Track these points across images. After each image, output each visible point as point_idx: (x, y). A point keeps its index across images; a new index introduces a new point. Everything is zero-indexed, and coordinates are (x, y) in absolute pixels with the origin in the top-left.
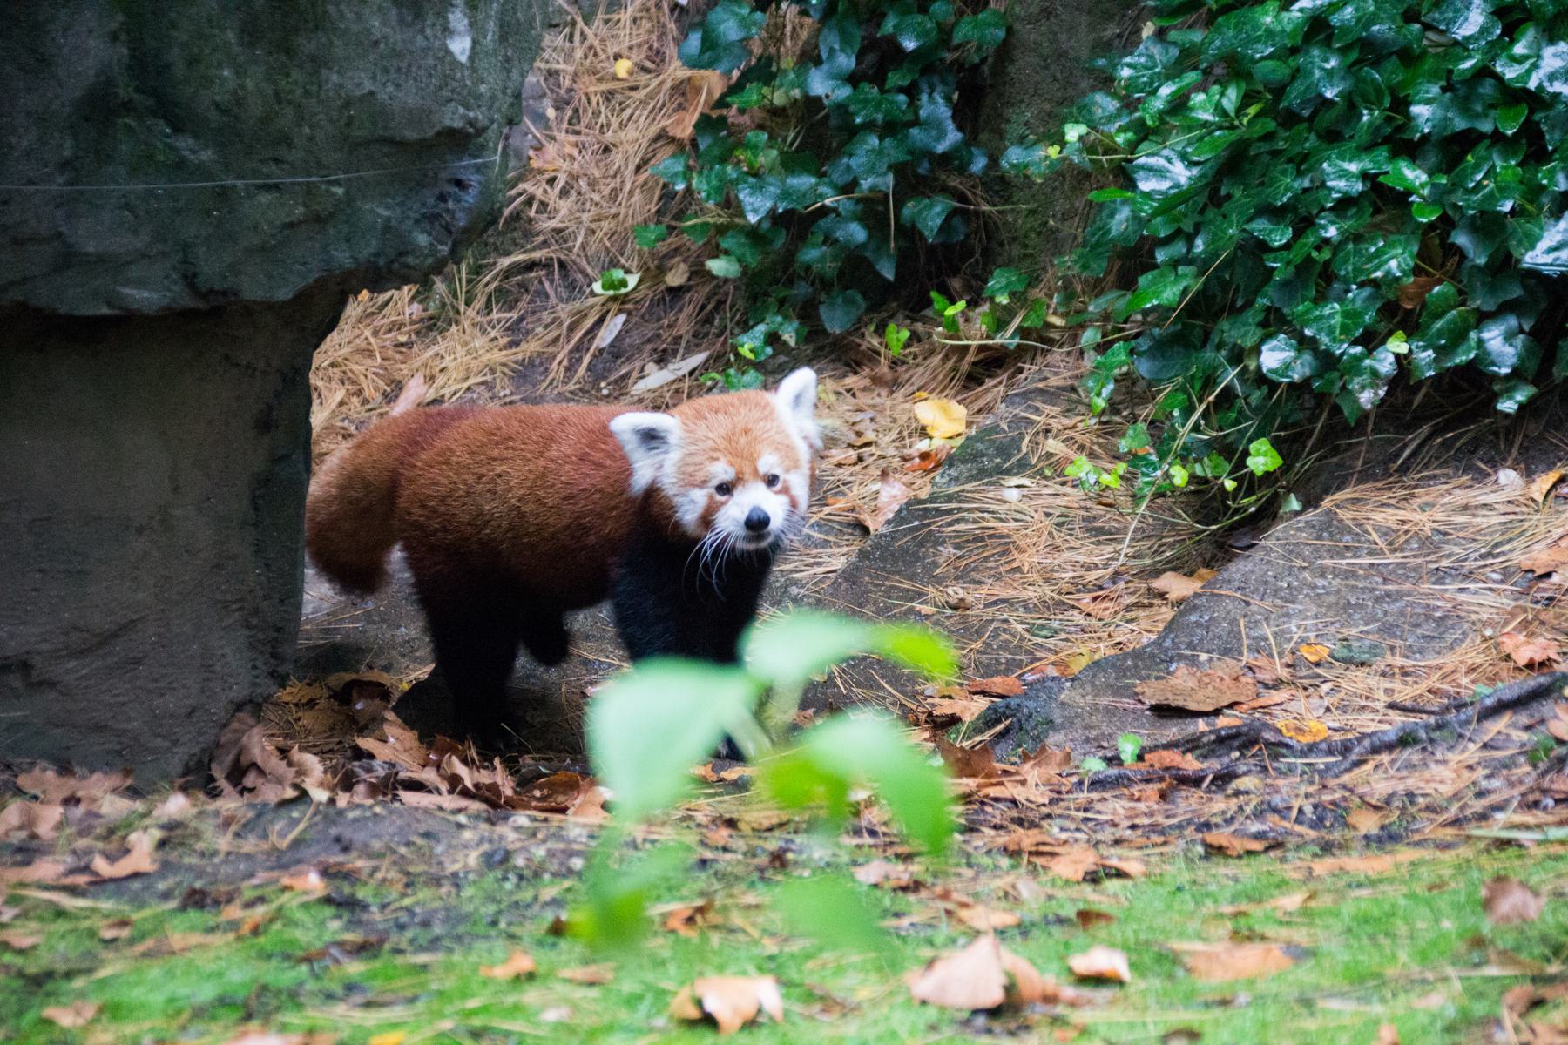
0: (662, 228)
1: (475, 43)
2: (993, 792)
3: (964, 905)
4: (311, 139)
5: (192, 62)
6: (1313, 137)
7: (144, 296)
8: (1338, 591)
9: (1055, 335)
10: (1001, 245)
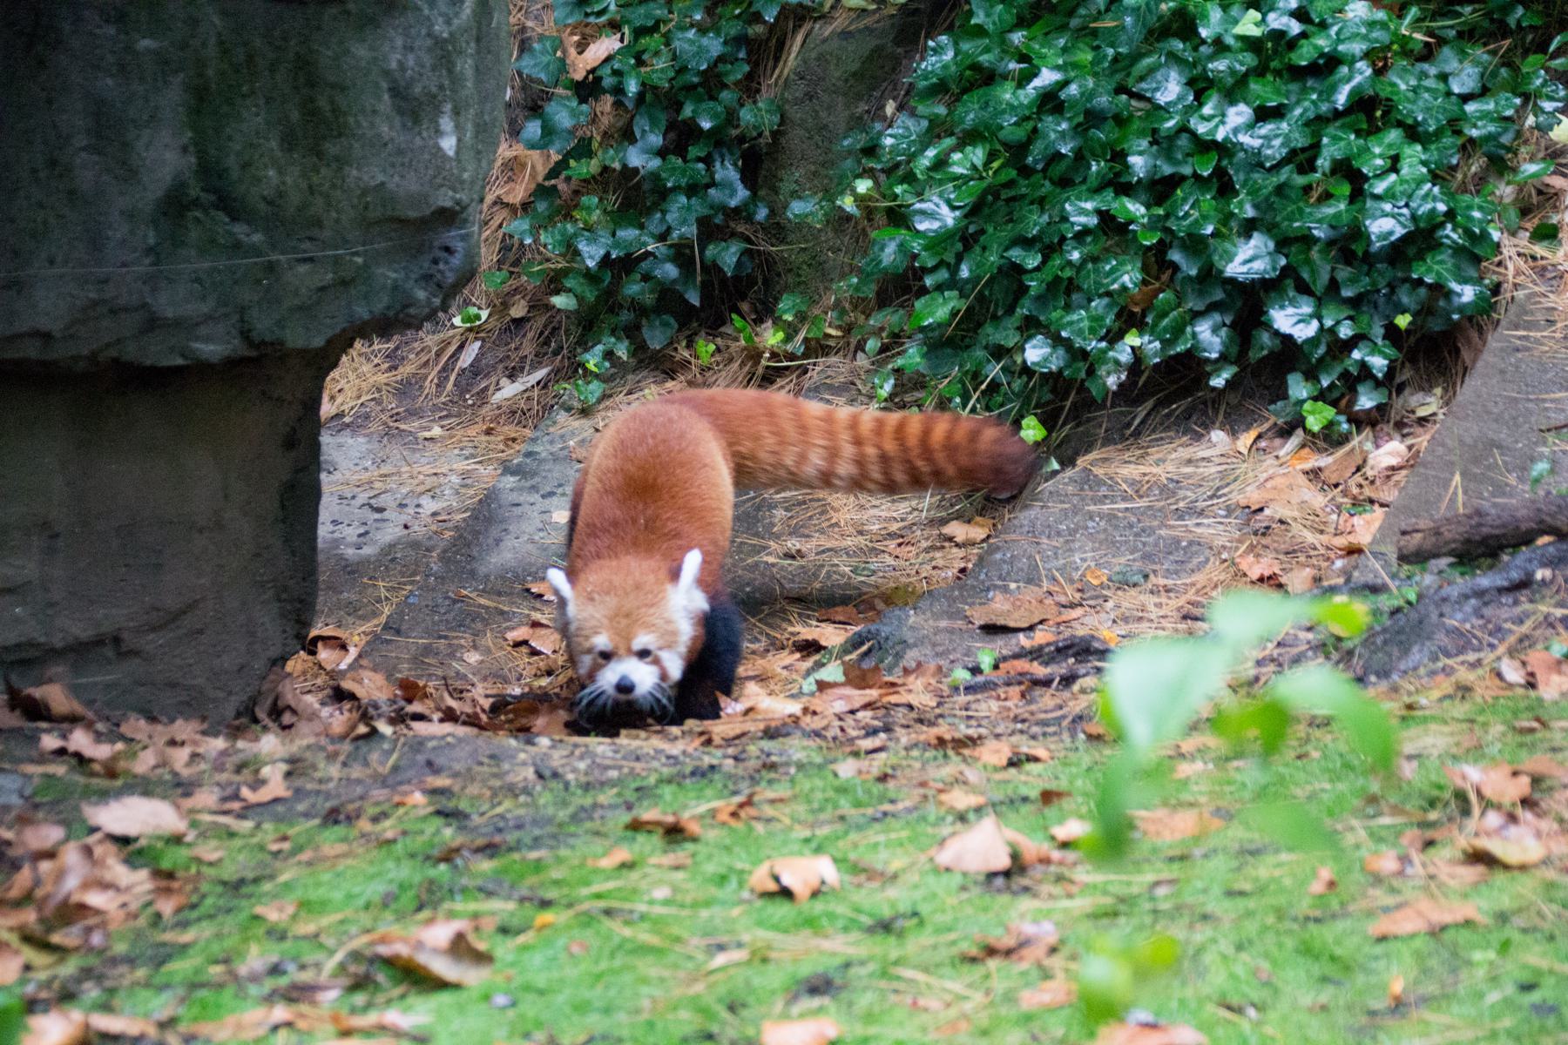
0: (505, 273)
1: (459, 140)
2: (893, 699)
3: (941, 791)
4: (337, 221)
5: (245, 166)
6: (1047, 183)
7: (212, 349)
9: (832, 343)
10: (779, 275)
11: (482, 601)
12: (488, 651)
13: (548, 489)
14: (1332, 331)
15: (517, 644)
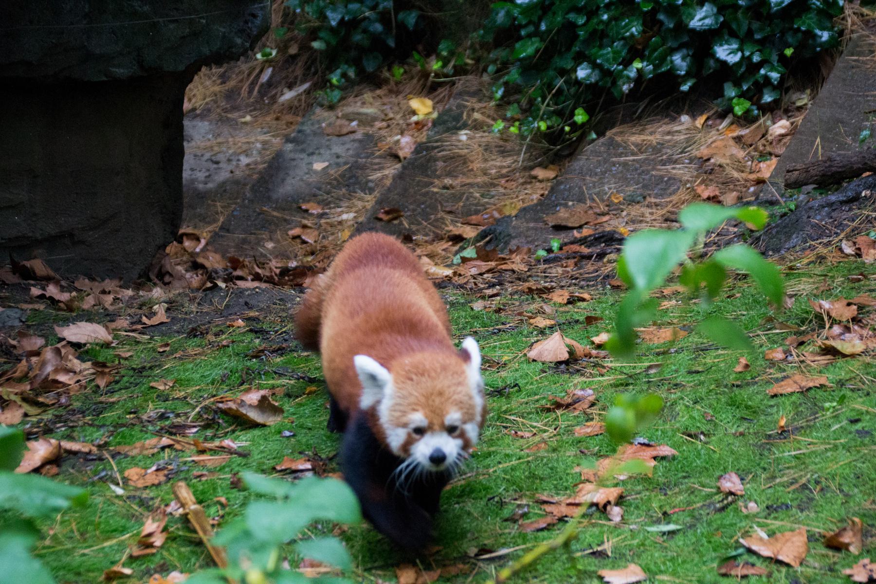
2: (504, 267)
3: (530, 318)
7: (120, 72)
8: (622, 172)
9: (469, 68)
11: (275, 214)
12: (277, 242)
13: (311, 151)
14: (749, 58)
15: (295, 238)
